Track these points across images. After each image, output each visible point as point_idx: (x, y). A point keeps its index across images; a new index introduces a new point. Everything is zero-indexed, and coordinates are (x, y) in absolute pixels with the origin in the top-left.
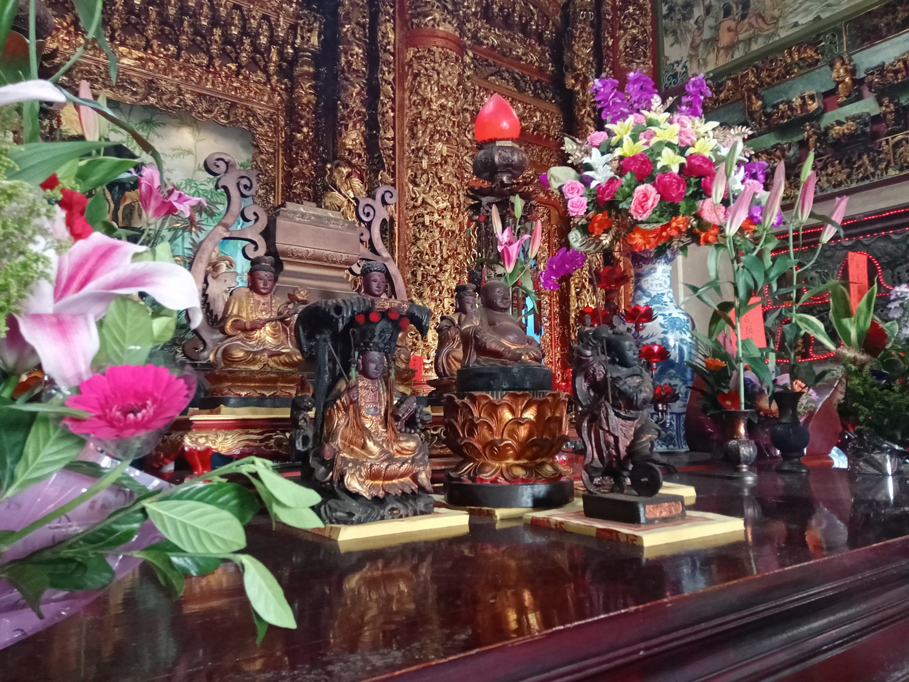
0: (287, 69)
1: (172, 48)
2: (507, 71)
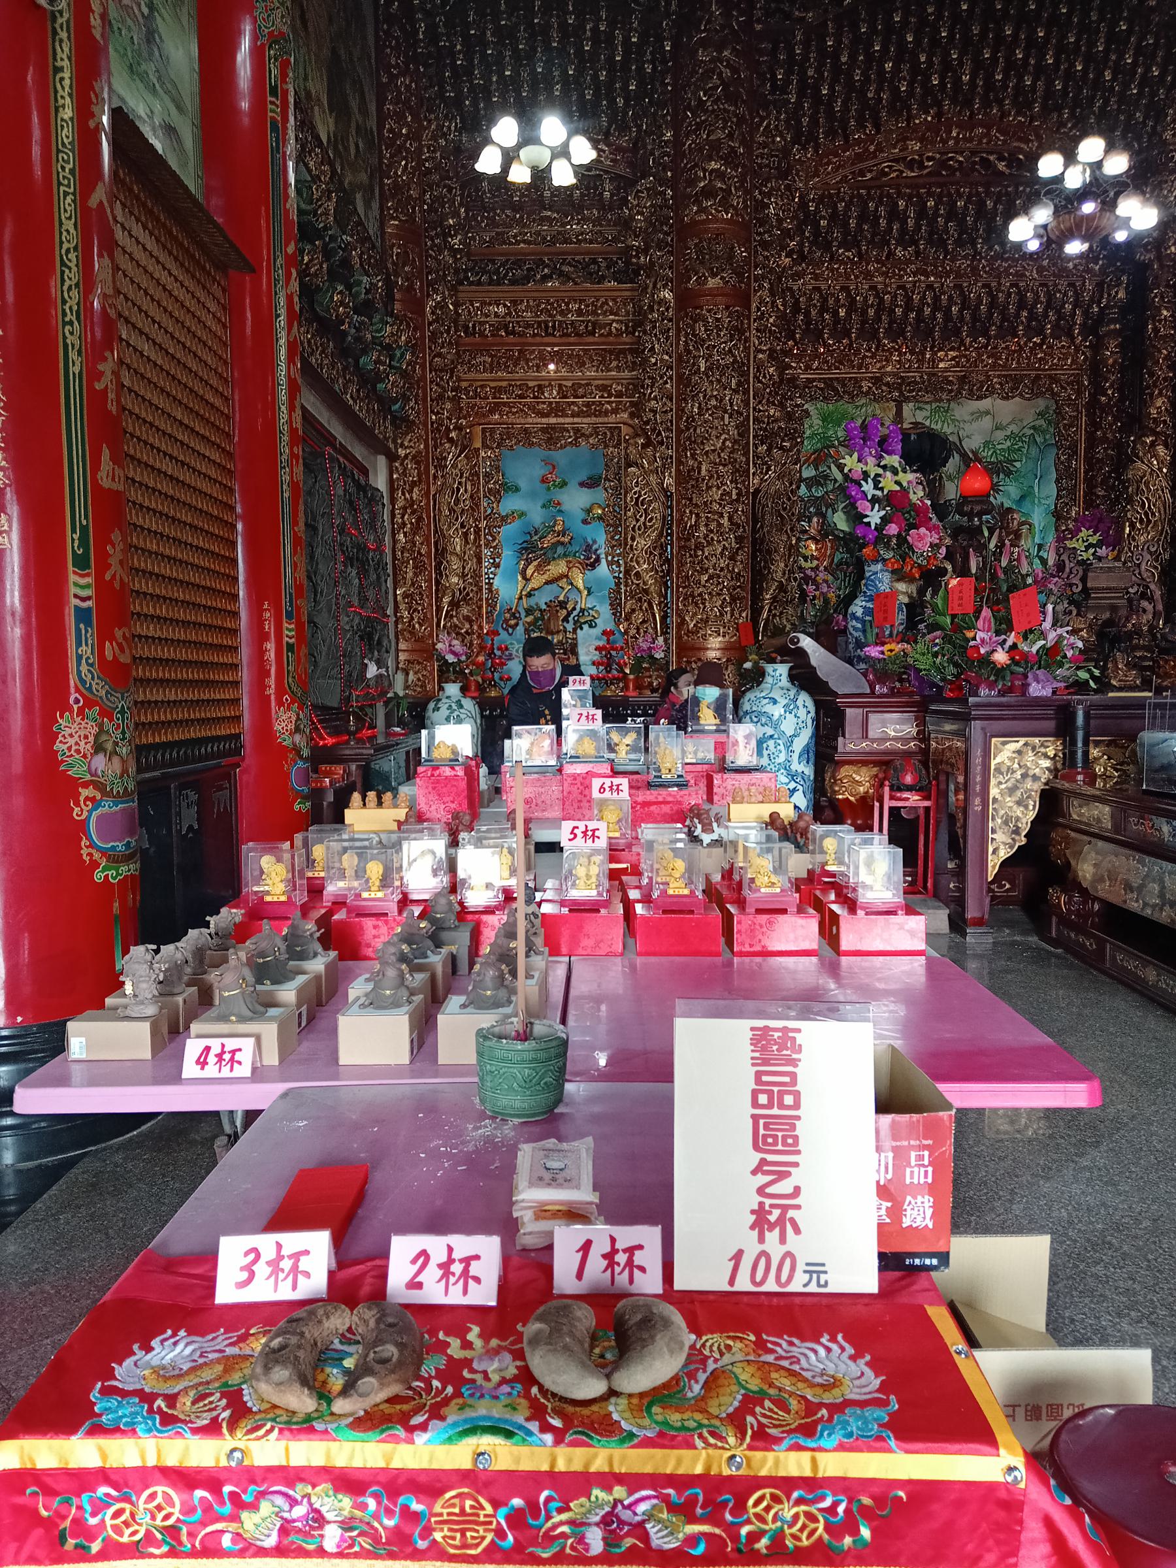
0: (1092, 327)
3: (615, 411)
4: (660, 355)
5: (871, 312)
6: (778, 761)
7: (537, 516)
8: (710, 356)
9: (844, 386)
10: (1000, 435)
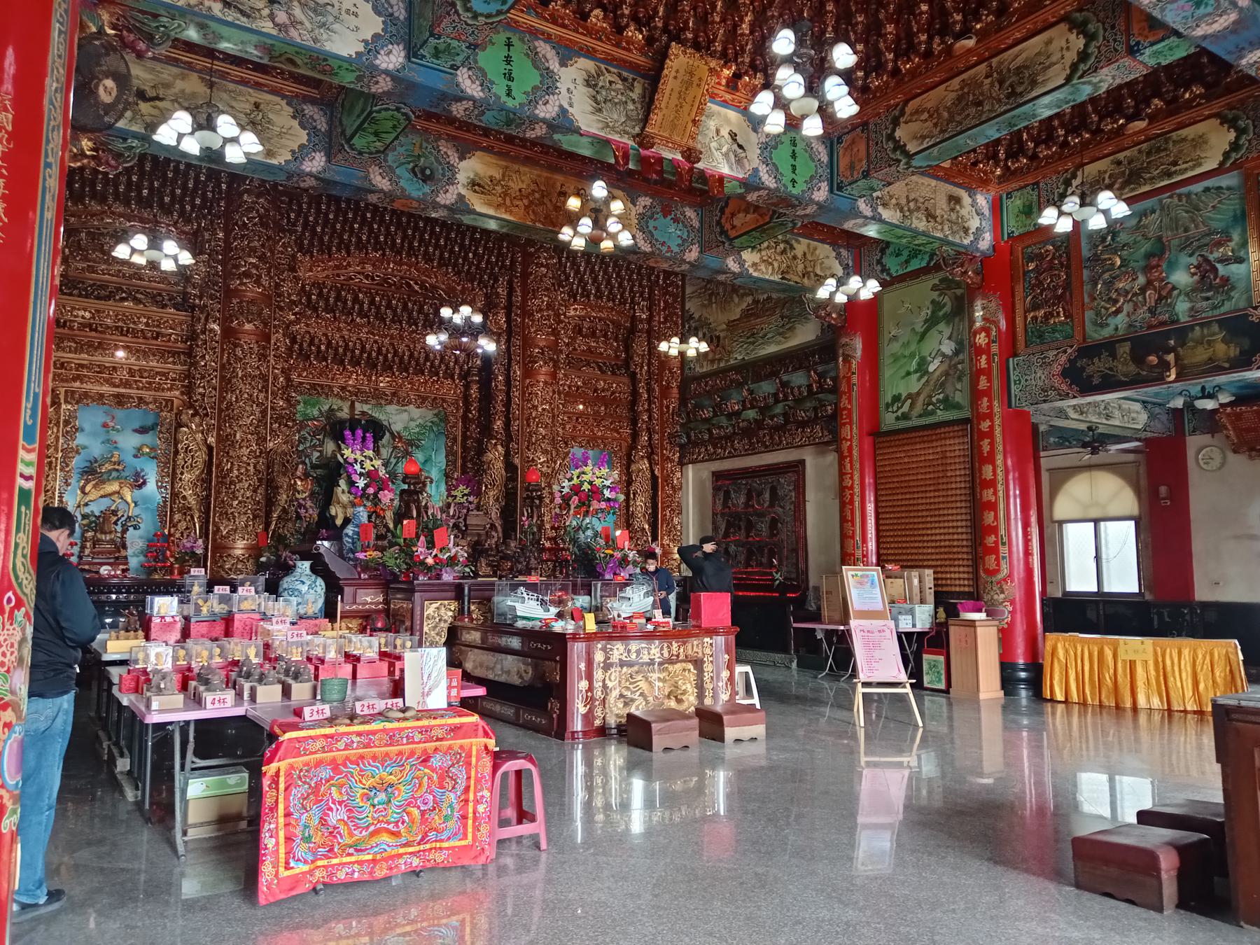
3: (170, 389)
4: (208, 361)
5: (341, 350)
7: (96, 449)
10: (413, 424)
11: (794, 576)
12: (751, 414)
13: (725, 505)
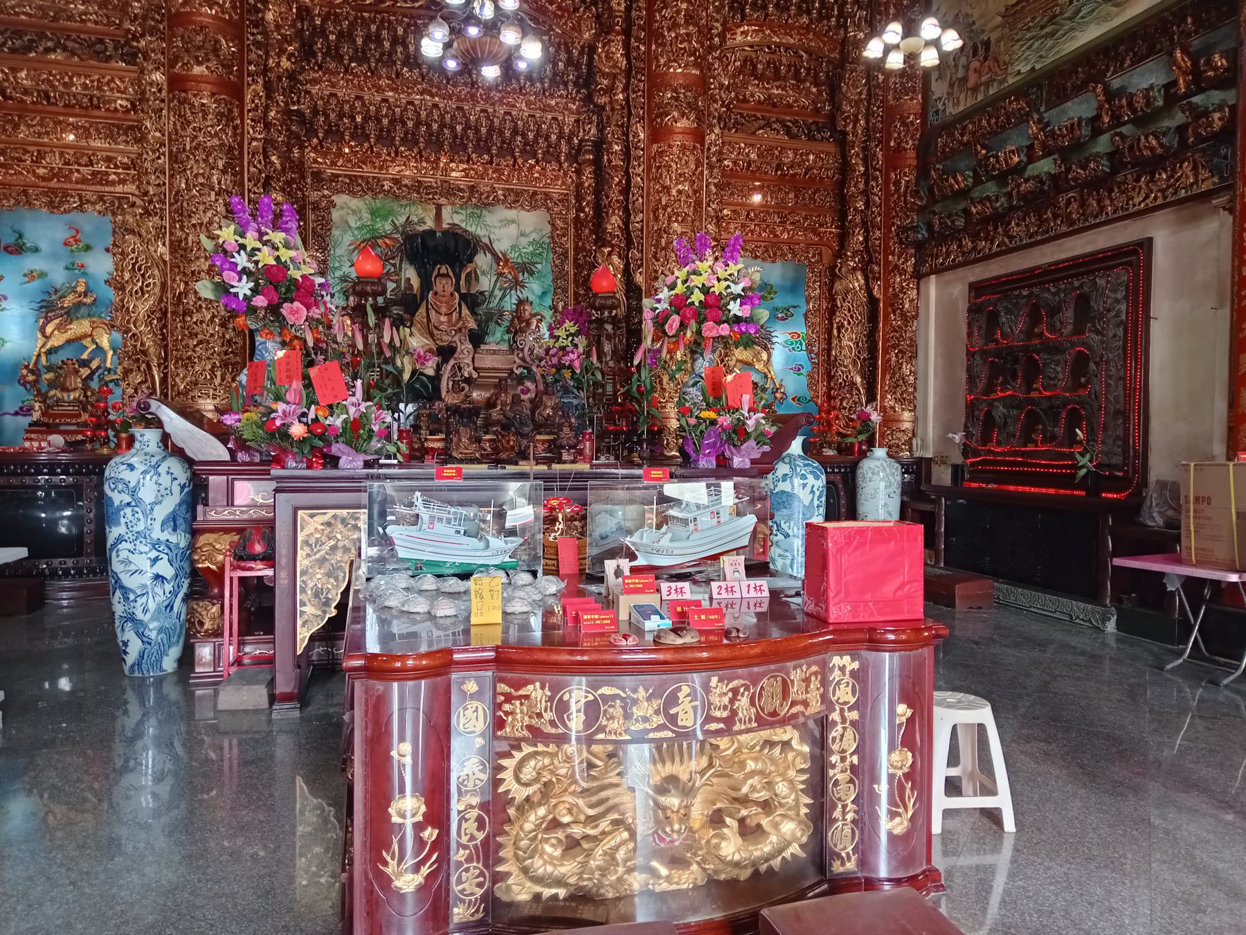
1: (486, 157)
2: (778, 121)
3: (122, 182)
6: (136, 529)
8: (196, 137)
9: (368, 183)
10: (524, 241)
11: (1117, 460)
12: (1045, 166)
13: (989, 336)
